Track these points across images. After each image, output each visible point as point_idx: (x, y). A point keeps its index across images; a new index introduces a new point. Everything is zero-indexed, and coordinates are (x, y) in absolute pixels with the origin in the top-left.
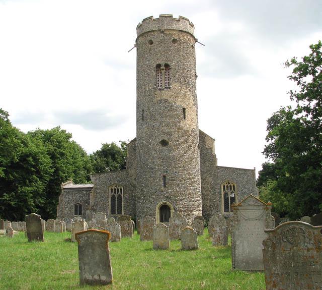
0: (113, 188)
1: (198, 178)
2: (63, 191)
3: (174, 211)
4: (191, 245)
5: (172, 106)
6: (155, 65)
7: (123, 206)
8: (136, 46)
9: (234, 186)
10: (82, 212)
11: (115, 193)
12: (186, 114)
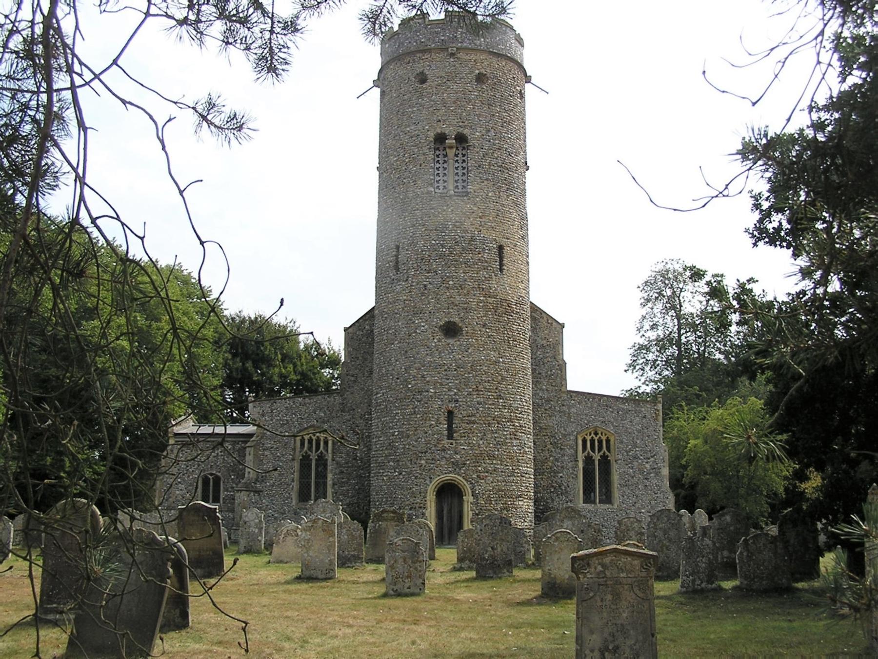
0: (306, 437)
1: (527, 419)
2: (171, 441)
3: (471, 499)
4: (328, 576)
5: (473, 239)
6: (432, 135)
7: (329, 482)
8: (376, 84)
9: (608, 441)
10: (222, 496)
11: (310, 448)
12: (505, 261)
